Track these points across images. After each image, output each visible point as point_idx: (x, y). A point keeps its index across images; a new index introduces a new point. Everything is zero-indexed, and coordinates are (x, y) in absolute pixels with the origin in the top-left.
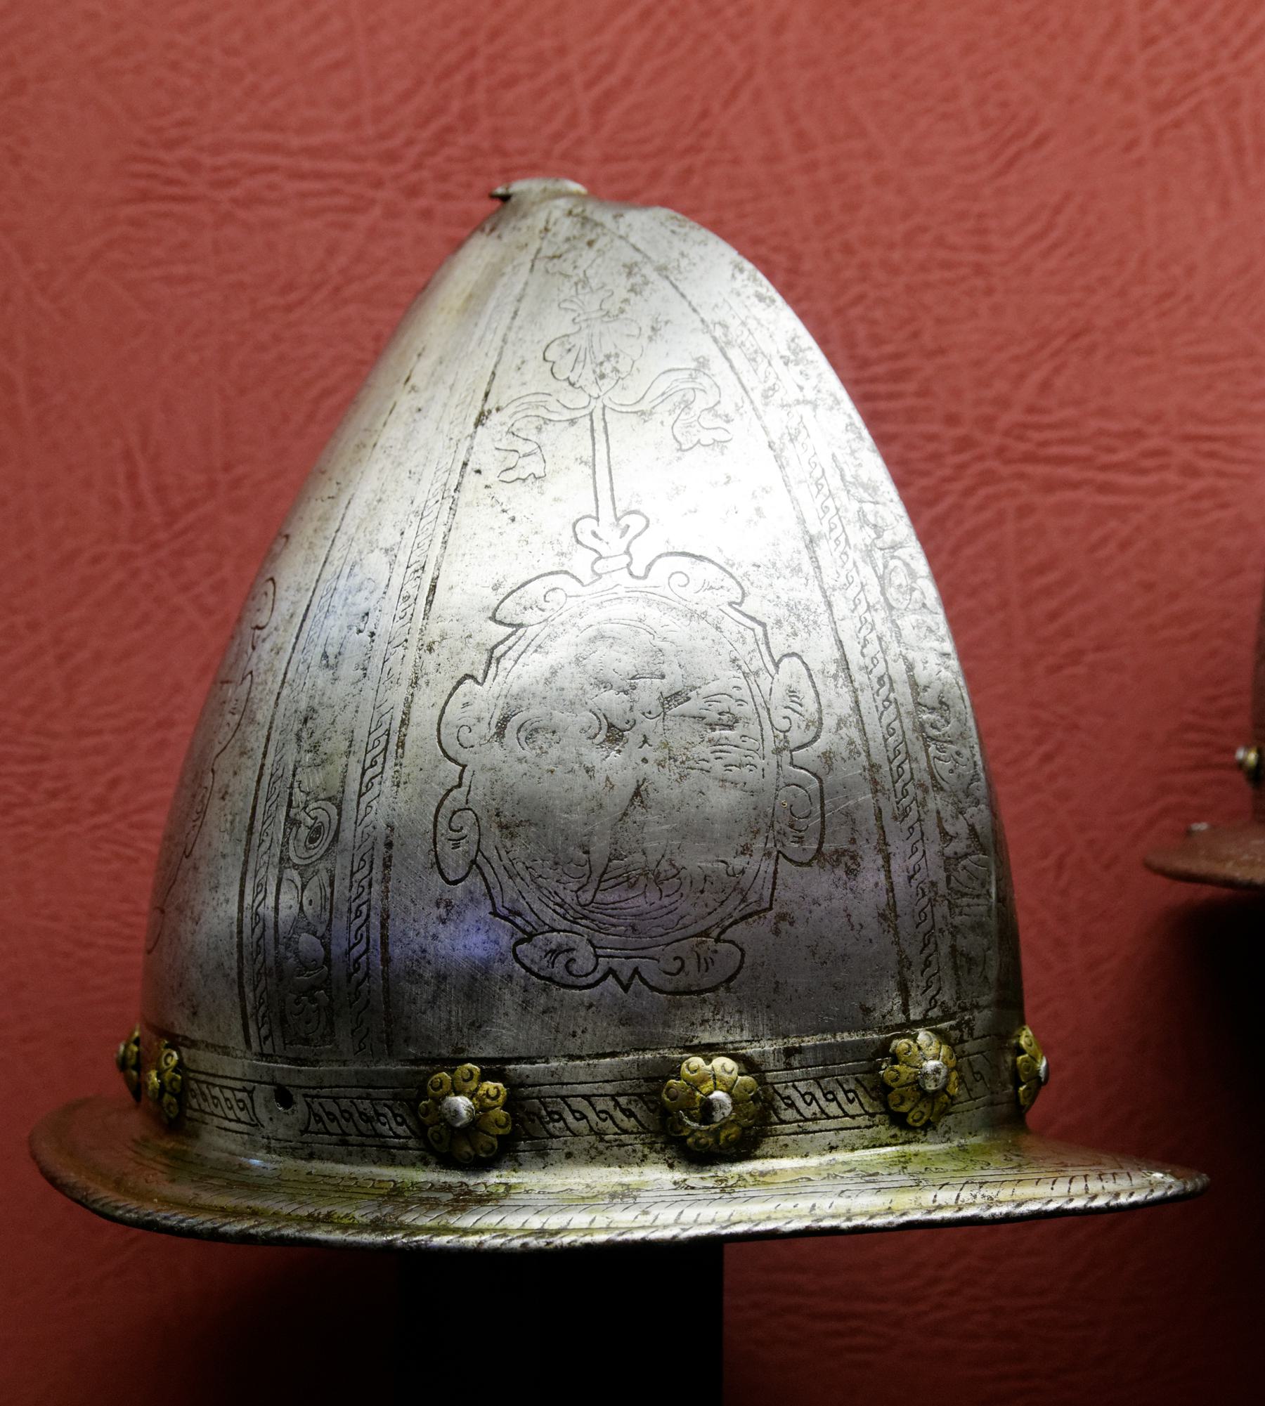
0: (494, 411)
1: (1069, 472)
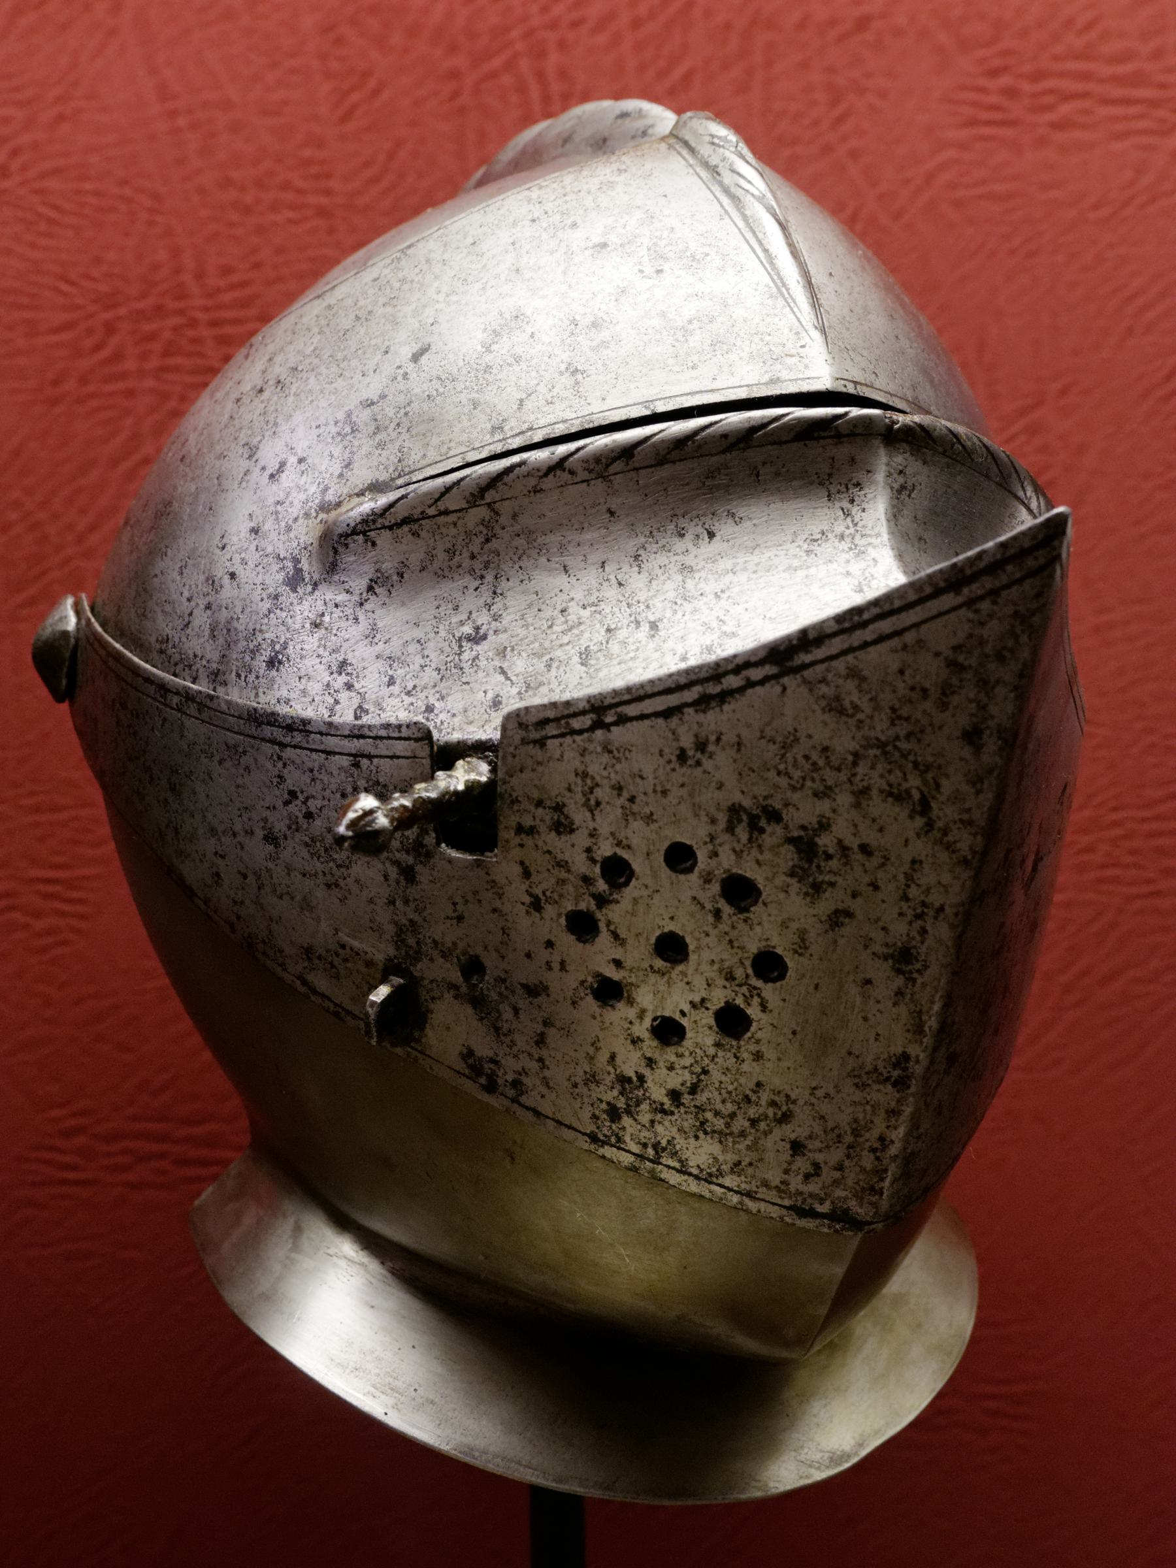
0: (647, 1072)
1: (1117, 92)
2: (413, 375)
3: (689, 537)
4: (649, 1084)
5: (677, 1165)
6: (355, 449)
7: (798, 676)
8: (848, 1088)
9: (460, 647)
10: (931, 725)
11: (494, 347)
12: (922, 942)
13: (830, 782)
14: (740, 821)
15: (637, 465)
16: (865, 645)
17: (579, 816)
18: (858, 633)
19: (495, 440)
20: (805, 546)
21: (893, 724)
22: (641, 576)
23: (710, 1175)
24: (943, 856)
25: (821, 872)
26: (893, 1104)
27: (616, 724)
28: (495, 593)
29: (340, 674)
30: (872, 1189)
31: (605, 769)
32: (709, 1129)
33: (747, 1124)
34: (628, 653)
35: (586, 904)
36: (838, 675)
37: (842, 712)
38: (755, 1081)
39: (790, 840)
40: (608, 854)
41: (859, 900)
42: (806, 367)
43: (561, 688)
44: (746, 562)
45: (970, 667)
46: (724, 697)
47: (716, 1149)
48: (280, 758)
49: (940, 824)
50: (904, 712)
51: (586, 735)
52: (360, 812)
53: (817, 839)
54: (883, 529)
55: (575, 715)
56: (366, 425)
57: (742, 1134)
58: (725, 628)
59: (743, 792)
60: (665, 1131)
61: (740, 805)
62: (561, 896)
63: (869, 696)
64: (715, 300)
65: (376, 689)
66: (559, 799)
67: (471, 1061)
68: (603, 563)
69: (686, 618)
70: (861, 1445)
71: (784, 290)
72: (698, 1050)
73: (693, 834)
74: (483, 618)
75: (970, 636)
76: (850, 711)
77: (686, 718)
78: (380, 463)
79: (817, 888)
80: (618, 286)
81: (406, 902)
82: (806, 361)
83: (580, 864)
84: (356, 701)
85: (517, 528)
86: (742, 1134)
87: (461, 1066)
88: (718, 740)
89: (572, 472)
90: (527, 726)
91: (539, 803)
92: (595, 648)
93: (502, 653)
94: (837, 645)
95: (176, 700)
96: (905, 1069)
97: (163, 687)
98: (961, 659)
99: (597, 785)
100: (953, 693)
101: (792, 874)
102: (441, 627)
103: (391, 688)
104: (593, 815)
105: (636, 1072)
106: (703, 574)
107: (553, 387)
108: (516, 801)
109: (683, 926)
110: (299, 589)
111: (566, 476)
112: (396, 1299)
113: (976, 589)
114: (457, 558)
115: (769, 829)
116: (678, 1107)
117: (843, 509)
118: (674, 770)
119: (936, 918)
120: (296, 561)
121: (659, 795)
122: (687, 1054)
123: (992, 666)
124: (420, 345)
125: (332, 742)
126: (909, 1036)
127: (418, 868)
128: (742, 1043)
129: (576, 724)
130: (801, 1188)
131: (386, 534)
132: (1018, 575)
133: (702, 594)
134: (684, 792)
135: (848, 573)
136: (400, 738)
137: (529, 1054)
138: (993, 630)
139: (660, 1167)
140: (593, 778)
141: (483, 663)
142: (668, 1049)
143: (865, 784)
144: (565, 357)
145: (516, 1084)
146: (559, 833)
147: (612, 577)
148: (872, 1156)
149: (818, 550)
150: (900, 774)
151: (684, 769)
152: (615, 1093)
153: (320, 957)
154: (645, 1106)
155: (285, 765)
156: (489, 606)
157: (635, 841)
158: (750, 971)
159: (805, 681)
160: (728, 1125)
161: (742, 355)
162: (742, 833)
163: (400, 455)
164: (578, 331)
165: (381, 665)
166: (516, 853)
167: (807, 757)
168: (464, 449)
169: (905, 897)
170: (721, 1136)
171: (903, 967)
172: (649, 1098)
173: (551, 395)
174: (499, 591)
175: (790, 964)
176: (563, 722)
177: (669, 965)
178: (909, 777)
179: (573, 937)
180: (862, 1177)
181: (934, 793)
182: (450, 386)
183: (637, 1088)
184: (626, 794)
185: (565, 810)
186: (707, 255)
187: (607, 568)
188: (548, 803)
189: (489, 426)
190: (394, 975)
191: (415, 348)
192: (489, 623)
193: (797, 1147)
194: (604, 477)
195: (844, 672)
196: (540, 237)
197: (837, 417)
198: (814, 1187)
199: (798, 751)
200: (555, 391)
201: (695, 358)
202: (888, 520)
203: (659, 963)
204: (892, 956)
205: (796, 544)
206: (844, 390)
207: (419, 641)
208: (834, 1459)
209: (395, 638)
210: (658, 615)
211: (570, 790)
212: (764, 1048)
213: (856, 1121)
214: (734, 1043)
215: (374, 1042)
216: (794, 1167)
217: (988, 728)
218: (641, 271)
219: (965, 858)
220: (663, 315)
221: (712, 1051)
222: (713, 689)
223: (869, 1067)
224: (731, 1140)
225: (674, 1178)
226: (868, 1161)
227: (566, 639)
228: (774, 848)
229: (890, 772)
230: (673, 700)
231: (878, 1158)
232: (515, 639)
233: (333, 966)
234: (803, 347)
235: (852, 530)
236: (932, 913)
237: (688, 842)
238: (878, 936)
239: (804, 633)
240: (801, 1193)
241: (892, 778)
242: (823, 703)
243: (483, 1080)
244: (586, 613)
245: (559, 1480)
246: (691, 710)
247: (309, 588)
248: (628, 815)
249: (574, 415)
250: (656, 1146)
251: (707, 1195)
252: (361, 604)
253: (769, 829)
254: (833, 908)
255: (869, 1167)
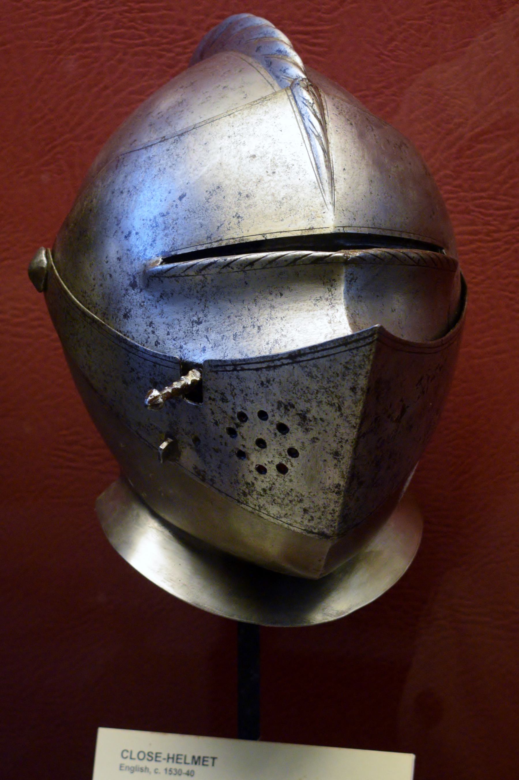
2: (179, 206)
3: (274, 294)
4: (256, 486)
5: (266, 513)
6: (157, 234)
7: (298, 364)
8: (321, 494)
9: (193, 325)
10: (340, 384)
11: (210, 200)
12: (342, 450)
13: (310, 398)
14: (282, 406)
15: (255, 268)
16: (319, 358)
17: (229, 398)
18: (316, 354)
19: (208, 242)
20: (314, 302)
21: (328, 383)
22: (256, 307)
23: (277, 517)
24: (347, 424)
25: (308, 425)
26: (336, 499)
27: (241, 370)
28: (205, 306)
29: (150, 326)
30: (331, 526)
31: (237, 384)
32: (276, 502)
33: (289, 502)
34: (249, 338)
35: (233, 426)
36: (310, 365)
37: (312, 377)
38: (290, 488)
39: (298, 414)
40: (240, 411)
41: (321, 435)
42: (324, 222)
43: (226, 348)
44: (293, 306)
45: (351, 369)
46: (275, 367)
47: (279, 509)
48: (128, 356)
49: (345, 415)
50: (332, 379)
51: (231, 372)
52: (153, 397)
53: (306, 415)
54: (342, 297)
55: (227, 365)
56: (161, 225)
57: (287, 505)
58: (283, 333)
59: (282, 398)
60: (262, 501)
61: (281, 402)
62: (224, 422)
63: (320, 373)
64: (293, 189)
65: (163, 336)
66: (223, 391)
67: (196, 470)
68: (243, 301)
69: (270, 326)
70: (350, 609)
71: (320, 184)
72: (271, 477)
73: (267, 408)
74: (201, 315)
75: (350, 360)
76: (315, 377)
77: (263, 372)
78: (166, 244)
79: (307, 430)
80: (258, 179)
81: (173, 414)
82: (324, 219)
83: (230, 412)
84: (156, 339)
85: (213, 284)
86: (287, 505)
87: (193, 471)
88: (274, 380)
89: (232, 268)
90: (212, 366)
91: (216, 391)
92: (239, 334)
93: (207, 330)
94: (310, 357)
95: (89, 320)
96: (339, 489)
97: (84, 313)
98: (348, 366)
99: (235, 388)
100: (346, 376)
101: (299, 425)
102: (186, 315)
103: (168, 336)
104: (234, 398)
105: (251, 482)
106: (277, 309)
107: (230, 223)
108: (208, 389)
109: (264, 436)
110: (135, 289)
111: (230, 269)
112: (175, 546)
113: (352, 346)
114: (192, 291)
115: (291, 410)
116: (265, 494)
117: (328, 289)
118: (260, 387)
119: (346, 443)
120: (134, 277)
121: (255, 395)
122: (268, 477)
123: (358, 369)
124: (182, 193)
125: (146, 356)
126: (340, 478)
127: (177, 404)
128: (285, 476)
129: (228, 368)
130: (308, 524)
131: (166, 279)
132: (364, 344)
133: (276, 318)
134: (263, 395)
135: (327, 315)
136: (169, 361)
137: (216, 471)
138: (358, 359)
139: (261, 513)
140: (234, 387)
141: (200, 333)
142: (262, 475)
143: (321, 400)
144: (236, 209)
145: (212, 480)
146: (223, 402)
147: (246, 306)
148: (331, 515)
149: (318, 304)
150: (331, 398)
151: (263, 388)
152: (245, 487)
153: (143, 427)
154: (255, 493)
155: (130, 359)
156: (203, 311)
157: (248, 408)
158: (287, 453)
159: (300, 366)
160: (282, 502)
161: (301, 216)
162: (282, 409)
163: (173, 241)
164: (241, 198)
165: (164, 326)
166: (210, 406)
167: (302, 389)
168: (197, 244)
169: (335, 436)
170: (280, 505)
171: (336, 457)
172: (256, 490)
173: (229, 226)
174: (207, 306)
175: (300, 453)
176: (223, 367)
177: (260, 448)
178: (334, 399)
179: (229, 436)
180: (328, 522)
181: (342, 405)
182: (193, 215)
183: (252, 486)
184: (244, 393)
185: (225, 395)
186: (293, 165)
187: (245, 303)
188: (219, 392)
189: (206, 236)
190: (169, 438)
191: (180, 194)
192: (203, 318)
193: (305, 511)
194: (244, 271)
195: (312, 365)
196: (231, 147)
197: (326, 257)
198: (312, 524)
199: (299, 387)
200: (231, 224)
201: (283, 216)
202: (344, 293)
203: (257, 448)
204: (332, 453)
205: (311, 301)
206: (338, 231)
207: (178, 320)
208: (338, 613)
209: (170, 317)
210: (261, 324)
211: (226, 389)
212: (293, 478)
213: (324, 504)
214: (283, 475)
215: (162, 462)
216: (305, 517)
217: (358, 387)
218: (267, 172)
219: (353, 425)
220: (273, 195)
221: (276, 477)
222: (272, 364)
223: (327, 487)
224: (283, 506)
225: (266, 517)
226: (329, 517)
227: (229, 328)
228: (292, 416)
229: (328, 397)
230: (259, 366)
231: (332, 516)
232: (211, 325)
233: (148, 430)
234: (324, 213)
235: (331, 297)
236: (344, 441)
237: (265, 411)
238: (328, 447)
239: (299, 350)
240: (308, 526)
241: (329, 399)
242: (306, 374)
243: (201, 477)
244: (236, 319)
245: (231, 616)
246: (265, 370)
247: (139, 290)
248: (245, 400)
249: (237, 237)
250: (259, 506)
251: (277, 523)
252: (158, 302)
253: (291, 410)
254: (312, 437)
255: (330, 519)
